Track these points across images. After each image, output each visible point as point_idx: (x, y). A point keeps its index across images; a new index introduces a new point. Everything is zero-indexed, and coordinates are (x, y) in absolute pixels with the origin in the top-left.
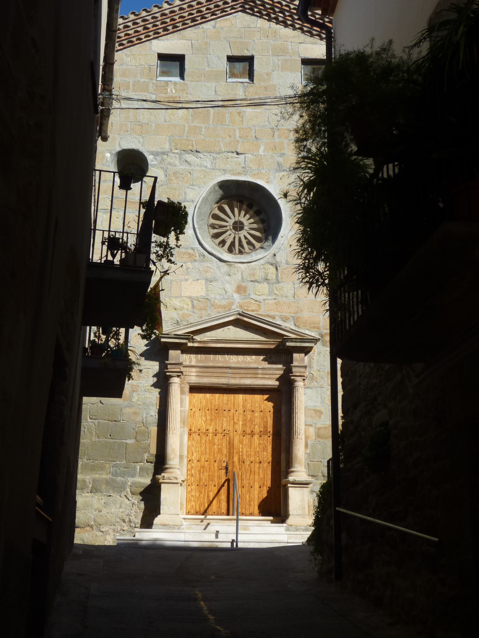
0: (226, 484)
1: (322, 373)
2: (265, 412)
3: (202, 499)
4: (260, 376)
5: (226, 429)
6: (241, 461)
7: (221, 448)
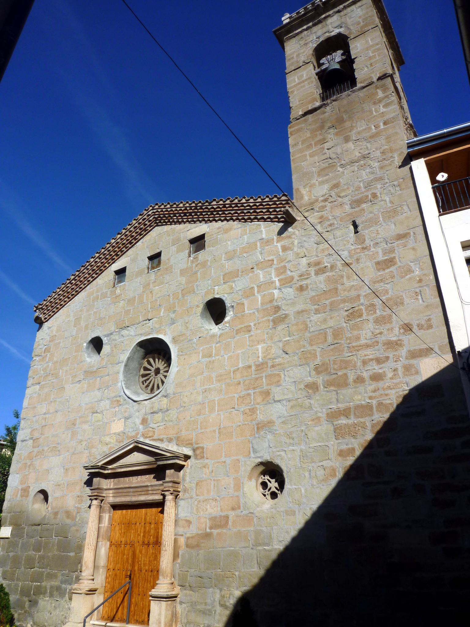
4: (150, 492)
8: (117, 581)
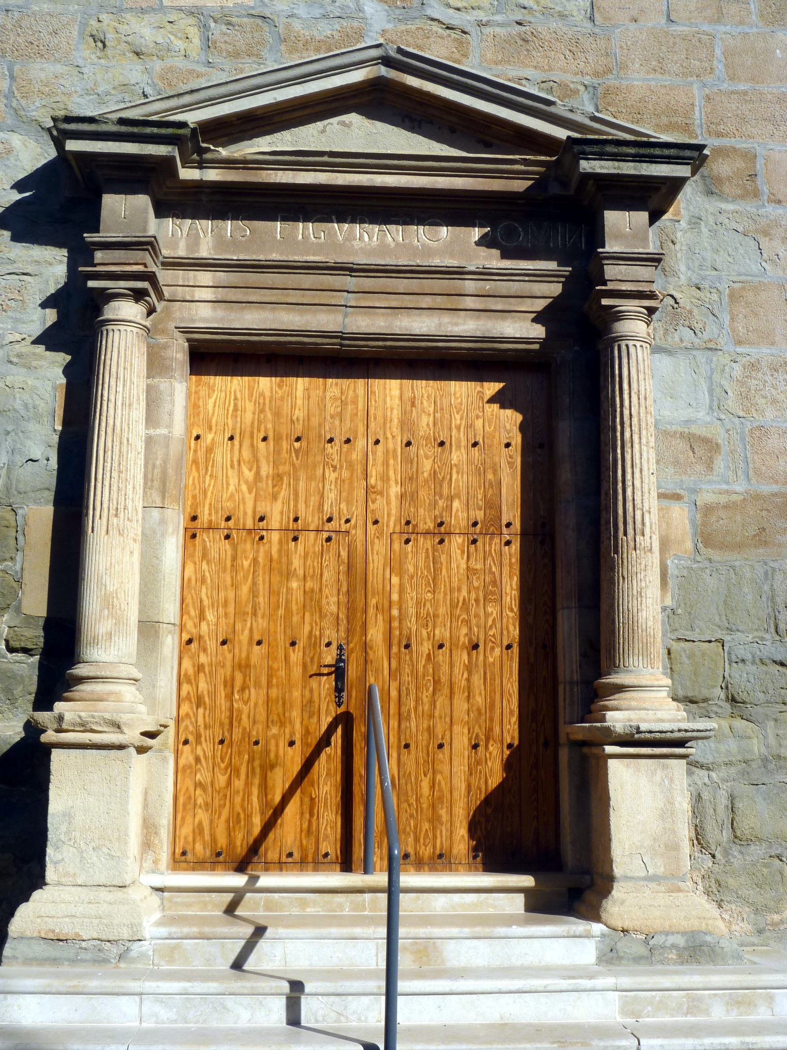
0: (337, 738)
1: (708, 295)
2: (490, 446)
3: (238, 800)
4: (470, 302)
5: (335, 516)
6: (395, 641)
7: (317, 588)
8: (256, 695)
